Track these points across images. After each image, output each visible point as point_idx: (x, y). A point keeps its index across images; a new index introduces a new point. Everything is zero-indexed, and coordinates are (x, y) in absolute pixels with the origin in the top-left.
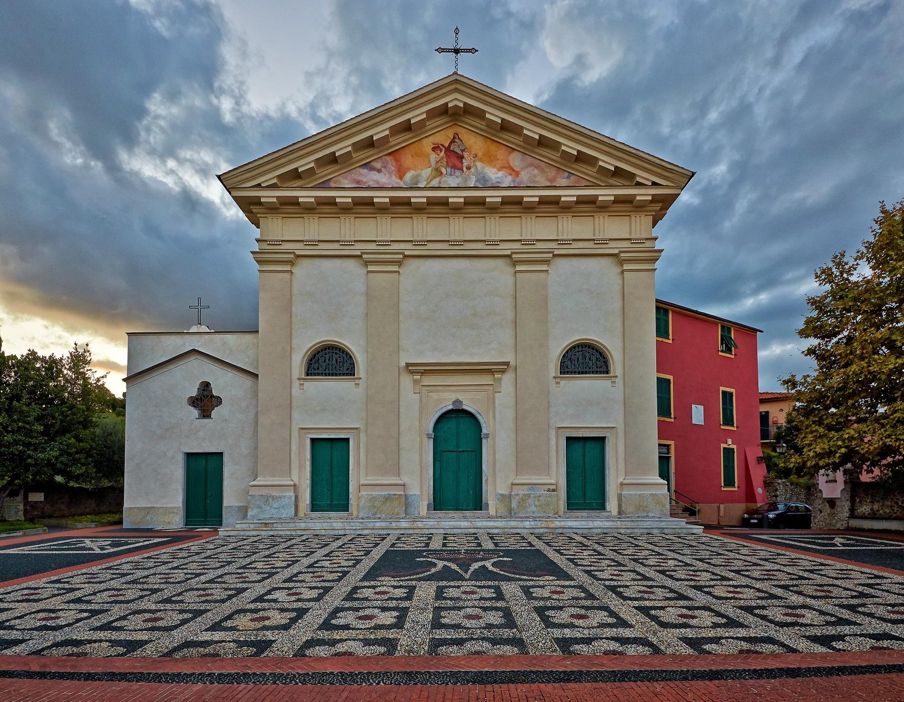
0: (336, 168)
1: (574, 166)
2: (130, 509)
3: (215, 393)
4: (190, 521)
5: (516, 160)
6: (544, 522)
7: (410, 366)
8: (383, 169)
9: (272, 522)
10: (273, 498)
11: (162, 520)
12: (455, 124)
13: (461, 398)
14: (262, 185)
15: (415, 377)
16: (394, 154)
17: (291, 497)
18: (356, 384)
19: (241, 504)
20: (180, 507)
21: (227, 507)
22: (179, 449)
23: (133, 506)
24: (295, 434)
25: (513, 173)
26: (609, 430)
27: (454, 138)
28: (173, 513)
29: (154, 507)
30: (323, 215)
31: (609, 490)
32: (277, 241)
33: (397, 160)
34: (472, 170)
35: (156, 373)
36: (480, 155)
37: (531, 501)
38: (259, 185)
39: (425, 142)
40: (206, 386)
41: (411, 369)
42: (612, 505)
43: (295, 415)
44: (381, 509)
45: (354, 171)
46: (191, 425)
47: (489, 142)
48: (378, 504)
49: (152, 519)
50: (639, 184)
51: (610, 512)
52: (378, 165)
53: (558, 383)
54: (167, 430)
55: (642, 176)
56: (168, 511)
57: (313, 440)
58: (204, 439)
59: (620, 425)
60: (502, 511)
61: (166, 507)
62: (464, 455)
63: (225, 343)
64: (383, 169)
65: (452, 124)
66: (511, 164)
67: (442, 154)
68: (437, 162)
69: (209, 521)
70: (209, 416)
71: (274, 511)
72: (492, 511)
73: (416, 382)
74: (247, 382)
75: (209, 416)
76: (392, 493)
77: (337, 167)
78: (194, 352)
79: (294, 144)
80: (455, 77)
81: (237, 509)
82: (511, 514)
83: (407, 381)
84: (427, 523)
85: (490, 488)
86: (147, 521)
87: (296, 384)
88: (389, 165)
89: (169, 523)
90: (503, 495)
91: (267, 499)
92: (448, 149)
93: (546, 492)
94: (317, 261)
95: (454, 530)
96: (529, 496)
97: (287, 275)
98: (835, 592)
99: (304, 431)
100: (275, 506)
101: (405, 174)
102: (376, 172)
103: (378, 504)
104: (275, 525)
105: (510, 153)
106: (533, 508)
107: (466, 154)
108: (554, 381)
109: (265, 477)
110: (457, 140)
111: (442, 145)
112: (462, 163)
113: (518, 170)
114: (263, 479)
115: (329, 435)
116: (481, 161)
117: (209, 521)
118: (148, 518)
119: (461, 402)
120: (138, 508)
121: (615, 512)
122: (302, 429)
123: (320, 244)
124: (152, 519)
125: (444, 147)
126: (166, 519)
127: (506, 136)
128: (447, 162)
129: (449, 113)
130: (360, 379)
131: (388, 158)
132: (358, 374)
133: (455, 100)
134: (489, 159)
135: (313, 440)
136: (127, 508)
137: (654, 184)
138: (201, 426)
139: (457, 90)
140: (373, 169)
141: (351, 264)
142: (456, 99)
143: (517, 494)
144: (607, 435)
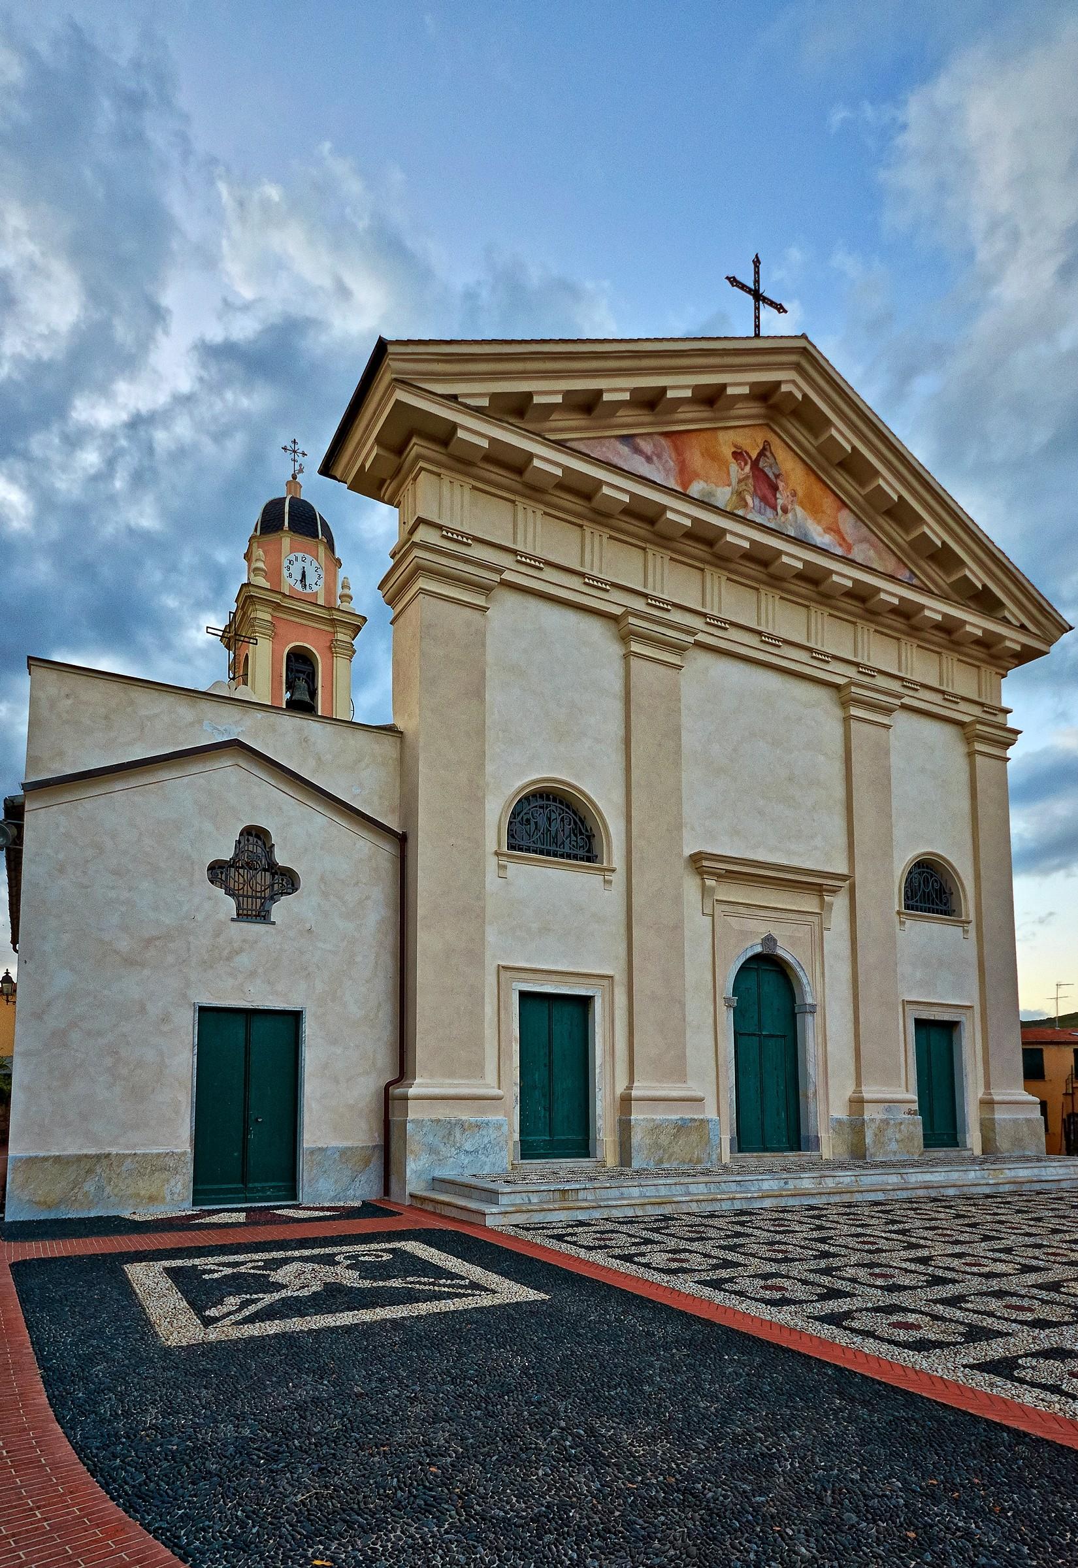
0: (583, 423)
1: (922, 563)
2: (31, 1161)
3: (281, 858)
4: (204, 1192)
5: (846, 521)
6: (991, 1172)
7: (707, 859)
8: (655, 458)
9: (578, 1186)
10: (462, 1125)
11: (130, 1191)
12: (767, 425)
13: (775, 934)
14: (459, 400)
15: (708, 882)
16: (673, 438)
17: (501, 1125)
18: (605, 881)
19: (348, 1144)
20: (185, 1153)
21: (312, 1152)
22: (184, 996)
23: (42, 1154)
24: (491, 980)
25: (844, 545)
26: (964, 1011)
27: (764, 449)
28: (165, 1169)
29: (108, 1156)
30: (554, 512)
31: (967, 1111)
32: (463, 535)
33: (679, 451)
34: (790, 515)
35: (118, 786)
36: (800, 493)
37: (890, 1132)
38: (454, 398)
39: (722, 436)
40: (256, 835)
41: (698, 863)
42: (974, 1139)
43: (491, 936)
44: (671, 1150)
45: (606, 442)
46: (218, 936)
47: (812, 478)
48: (664, 1140)
49: (100, 1188)
50: (1006, 621)
51: (971, 1149)
52: (646, 446)
53: (902, 923)
54: (149, 942)
55: (1012, 611)
56: (154, 1165)
57: (523, 995)
58: (253, 974)
59: (976, 1002)
60: (842, 1153)
61: (144, 1155)
62: (771, 1043)
63: (306, 740)
64: (655, 458)
65: (760, 422)
66: (841, 527)
67: (747, 469)
68: (740, 481)
69: (252, 1190)
70: (262, 916)
71: (466, 1160)
72: (826, 1152)
73: (705, 891)
74: (361, 843)
75: (262, 916)
76: (686, 1117)
77: (582, 422)
78: (235, 746)
79: (656, 340)
80: (801, 343)
81: (337, 1156)
82: (858, 1155)
83: (691, 886)
84: (841, 1180)
85: (821, 1107)
86: (86, 1194)
87: (492, 862)
88: (666, 456)
89: (152, 1199)
90: (839, 1121)
91: (449, 1128)
92: (755, 464)
93: (906, 1116)
94: (534, 604)
95: (898, 1192)
96: (888, 1123)
97: (476, 615)
98: (712, 1233)
99: (509, 974)
100: (468, 1146)
101: (690, 482)
102: (643, 460)
103: (664, 1140)
104: (581, 1195)
105: (839, 510)
106: (894, 1146)
107: (781, 485)
108: (896, 918)
109: (432, 1076)
110: (768, 454)
111: (746, 452)
112: (776, 499)
113: (851, 542)
114: (429, 1081)
115: (557, 987)
116: (801, 504)
117: (252, 1190)
118: (89, 1187)
119: (775, 941)
120: (57, 1159)
121: (978, 1151)
122: (506, 968)
123: (547, 569)
124: (100, 1188)
125: (750, 458)
126: (144, 1187)
127: (842, 478)
128: (754, 487)
129: (771, 402)
130: (613, 871)
131: (663, 442)
132: (609, 861)
133: (791, 383)
134: (815, 510)
135: (523, 995)
136: (20, 1159)
137: (1023, 626)
138: (244, 941)
139: (798, 367)
140: (637, 450)
141: (595, 630)
142: (794, 382)
143: (873, 1119)
144: (963, 1019)
